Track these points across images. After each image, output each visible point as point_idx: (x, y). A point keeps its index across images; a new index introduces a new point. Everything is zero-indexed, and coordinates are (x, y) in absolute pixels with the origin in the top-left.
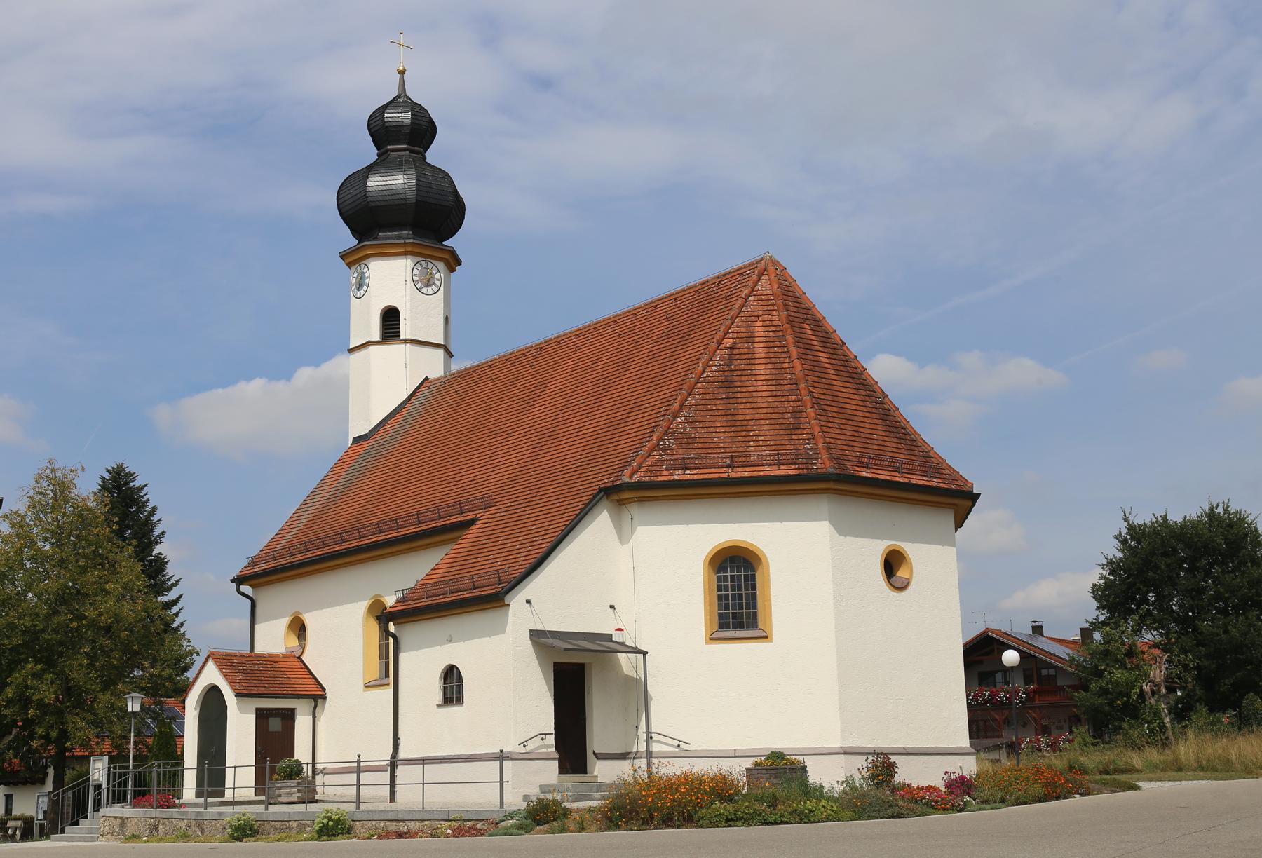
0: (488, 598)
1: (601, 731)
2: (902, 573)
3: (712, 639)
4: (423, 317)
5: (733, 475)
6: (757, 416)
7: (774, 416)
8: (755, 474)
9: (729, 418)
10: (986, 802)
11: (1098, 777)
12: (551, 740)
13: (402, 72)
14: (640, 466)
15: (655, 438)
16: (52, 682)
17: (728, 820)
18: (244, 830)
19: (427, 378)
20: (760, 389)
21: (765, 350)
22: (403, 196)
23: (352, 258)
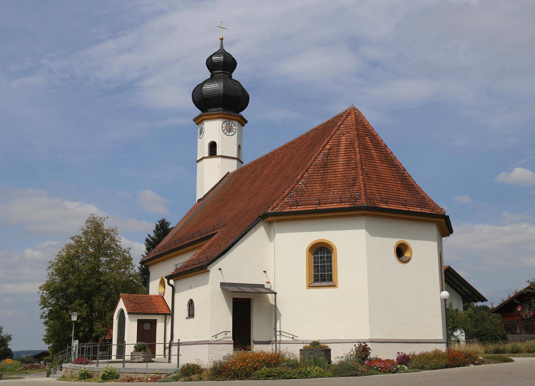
0: (198, 269)
1: (258, 331)
2: (407, 255)
3: (310, 286)
4: (228, 145)
5: (319, 208)
6: (336, 181)
7: (344, 180)
8: (329, 207)
9: (323, 181)
10: (413, 368)
11: (493, 355)
12: (230, 335)
13: (222, 39)
14: (277, 205)
15: (286, 192)
16: (86, 308)
17: (267, 376)
18: (84, 376)
19: (228, 173)
20: (339, 168)
21: (345, 150)
22: (218, 93)
23: (199, 121)
